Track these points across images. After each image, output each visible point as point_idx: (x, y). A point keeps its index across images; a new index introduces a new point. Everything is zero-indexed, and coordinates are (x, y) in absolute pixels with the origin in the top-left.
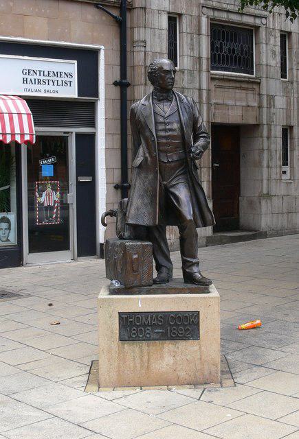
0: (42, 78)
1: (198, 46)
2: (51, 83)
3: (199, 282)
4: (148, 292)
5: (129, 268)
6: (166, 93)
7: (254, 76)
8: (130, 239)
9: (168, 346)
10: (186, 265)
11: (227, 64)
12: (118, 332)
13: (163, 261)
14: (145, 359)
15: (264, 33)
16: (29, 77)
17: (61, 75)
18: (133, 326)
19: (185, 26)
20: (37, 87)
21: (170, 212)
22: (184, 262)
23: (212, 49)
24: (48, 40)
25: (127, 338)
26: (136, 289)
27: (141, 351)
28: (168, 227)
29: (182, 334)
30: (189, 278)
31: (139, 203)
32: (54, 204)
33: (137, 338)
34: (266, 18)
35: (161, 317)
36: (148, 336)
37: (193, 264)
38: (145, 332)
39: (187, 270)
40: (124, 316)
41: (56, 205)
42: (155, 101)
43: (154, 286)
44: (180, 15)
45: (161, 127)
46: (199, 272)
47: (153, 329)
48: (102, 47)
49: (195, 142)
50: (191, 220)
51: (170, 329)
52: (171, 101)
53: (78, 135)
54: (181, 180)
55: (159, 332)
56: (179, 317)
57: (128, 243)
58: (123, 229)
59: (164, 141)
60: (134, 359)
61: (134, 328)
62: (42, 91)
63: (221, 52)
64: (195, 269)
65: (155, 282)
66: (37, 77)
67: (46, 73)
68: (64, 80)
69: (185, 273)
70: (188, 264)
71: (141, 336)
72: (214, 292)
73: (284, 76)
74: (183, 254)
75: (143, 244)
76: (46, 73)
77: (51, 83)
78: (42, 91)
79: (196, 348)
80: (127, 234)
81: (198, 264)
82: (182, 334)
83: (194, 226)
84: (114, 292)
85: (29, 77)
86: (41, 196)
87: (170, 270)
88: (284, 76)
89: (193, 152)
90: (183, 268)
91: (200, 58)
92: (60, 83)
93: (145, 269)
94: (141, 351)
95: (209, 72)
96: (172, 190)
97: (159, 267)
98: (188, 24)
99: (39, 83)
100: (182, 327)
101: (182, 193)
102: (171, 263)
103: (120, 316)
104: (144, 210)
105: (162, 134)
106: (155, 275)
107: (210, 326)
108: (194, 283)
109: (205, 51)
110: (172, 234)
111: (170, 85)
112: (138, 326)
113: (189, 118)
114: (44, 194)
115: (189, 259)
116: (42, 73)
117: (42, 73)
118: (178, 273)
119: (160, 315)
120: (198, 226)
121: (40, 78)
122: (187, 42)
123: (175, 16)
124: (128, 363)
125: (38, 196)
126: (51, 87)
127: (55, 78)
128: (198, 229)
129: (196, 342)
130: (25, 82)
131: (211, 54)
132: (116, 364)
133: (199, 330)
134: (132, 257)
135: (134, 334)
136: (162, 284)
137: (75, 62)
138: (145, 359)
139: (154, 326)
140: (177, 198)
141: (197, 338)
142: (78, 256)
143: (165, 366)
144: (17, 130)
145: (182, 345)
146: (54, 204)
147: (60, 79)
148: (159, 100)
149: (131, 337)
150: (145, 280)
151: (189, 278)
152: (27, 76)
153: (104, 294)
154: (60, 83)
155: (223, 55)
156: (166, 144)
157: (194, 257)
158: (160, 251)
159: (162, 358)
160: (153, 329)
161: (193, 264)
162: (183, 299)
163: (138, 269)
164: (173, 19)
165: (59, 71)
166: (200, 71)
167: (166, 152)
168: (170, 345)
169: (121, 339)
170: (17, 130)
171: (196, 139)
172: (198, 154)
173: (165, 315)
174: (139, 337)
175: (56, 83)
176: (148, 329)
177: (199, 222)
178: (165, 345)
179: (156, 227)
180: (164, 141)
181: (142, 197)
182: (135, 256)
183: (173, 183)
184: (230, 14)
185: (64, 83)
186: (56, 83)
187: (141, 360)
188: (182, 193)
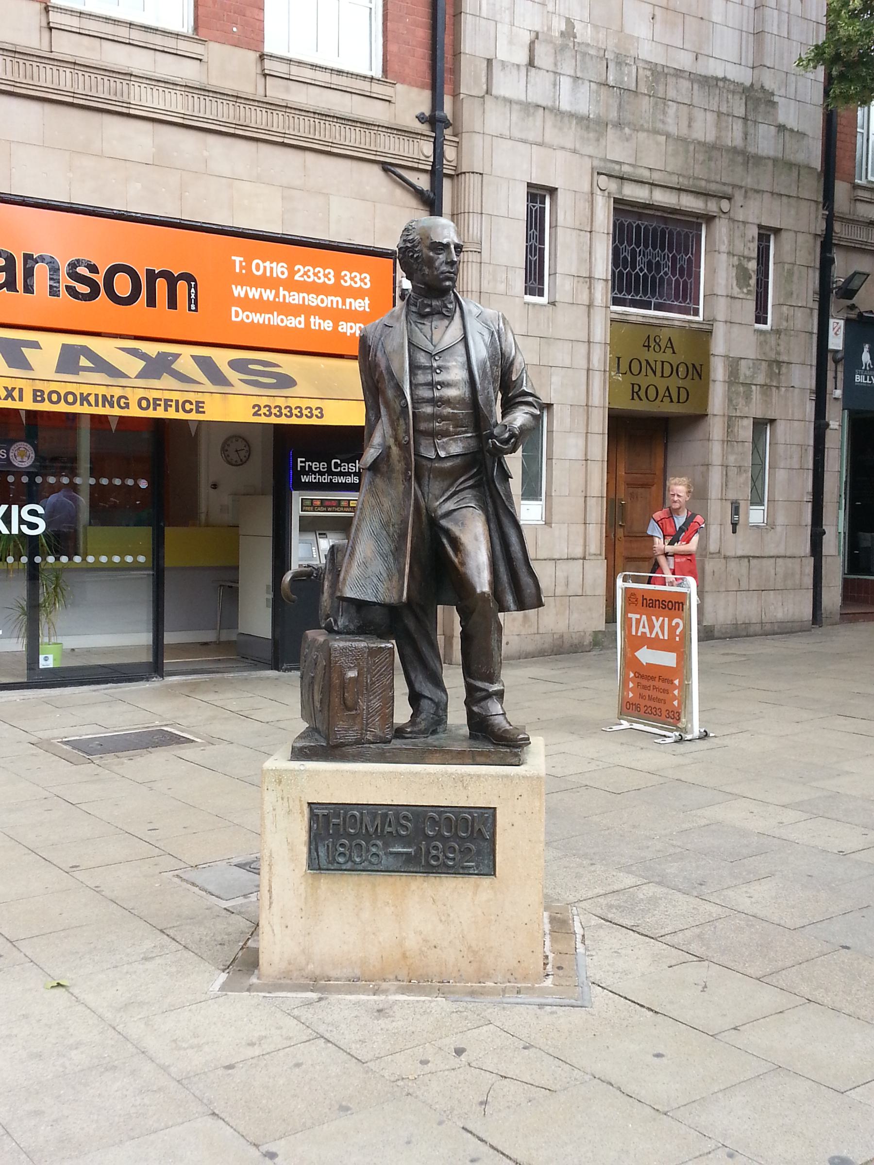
5: (336, 700)
6: (437, 297)
7: (700, 318)
8: (346, 632)
10: (474, 697)
11: (645, 293)
13: (426, 689)
18: (342, 836)
19: (564, 213)
22: (471, 690)
23: (615, 263)
26: (350, 750)
29: (454, 859)
31: (369, 553)
33: (349, 865)
34: (729, 199)
35: (405, 818)
37: (489, 696)
38: (368, 851)
39: (475, 709)
42: (414, 317)
43: (397, 743)
44: (552, 191)
45: (422, 378)
46: (506, 713)
49: (503, 417)
52: (451, 318)
54: (469, 499)
56: (448, 818)
57: (339, 644)
59: (428, 410)
61: (342, 839)
63: (634, 268)
64: (495, 707)
65: (399, 732)
69: (471, 715)
70: (479, 694)
73: (761, 318)
81: (500, 695)
82: (454, 859)
84: (300, 754)
87: (441, 708)
88: (761, 318)
89: (496, 438)
90: (466, 703)
93: (376, 704)
95: (607, 307)
96: (443, 522)
97: (415, 698)
100: (457, 843)
102: (444, 690)
103: (311, 810)
104: (378, 567)
105: (425, 393)
106: (402, 713)
108: (494, 741)
109: (603, 267)
110: (449, 621)
111: (449, 279)
113: (492, 357)
115: (479, 684)
118: (457, 716)
120: (503, 609)
123: (542, 192)
130: (193, 307)
131: (613, 273)
134: (342, 675)
136: (420, 739)
139: (389, 839)
140: (456, 543)
141: (491, 871)
148: (423, 316)
150: (376, 729)
153: (280, 761)
155: (637, 274)
156: (433, 417)
157: (492, 678)
158: (422, 664)
160: (386, 845)
161: (489, 696)
162: (461, 778)
164: (538, 195)
167: (433, 434)
169: (310, 867)
171: (508, 406)
172: (506, 442)
173: (349, 761)
174: (354, 862)
177: (509, 599)
180: (428, 410)
181: (377, 538)
182: (352, 674)
183: (450, 505)
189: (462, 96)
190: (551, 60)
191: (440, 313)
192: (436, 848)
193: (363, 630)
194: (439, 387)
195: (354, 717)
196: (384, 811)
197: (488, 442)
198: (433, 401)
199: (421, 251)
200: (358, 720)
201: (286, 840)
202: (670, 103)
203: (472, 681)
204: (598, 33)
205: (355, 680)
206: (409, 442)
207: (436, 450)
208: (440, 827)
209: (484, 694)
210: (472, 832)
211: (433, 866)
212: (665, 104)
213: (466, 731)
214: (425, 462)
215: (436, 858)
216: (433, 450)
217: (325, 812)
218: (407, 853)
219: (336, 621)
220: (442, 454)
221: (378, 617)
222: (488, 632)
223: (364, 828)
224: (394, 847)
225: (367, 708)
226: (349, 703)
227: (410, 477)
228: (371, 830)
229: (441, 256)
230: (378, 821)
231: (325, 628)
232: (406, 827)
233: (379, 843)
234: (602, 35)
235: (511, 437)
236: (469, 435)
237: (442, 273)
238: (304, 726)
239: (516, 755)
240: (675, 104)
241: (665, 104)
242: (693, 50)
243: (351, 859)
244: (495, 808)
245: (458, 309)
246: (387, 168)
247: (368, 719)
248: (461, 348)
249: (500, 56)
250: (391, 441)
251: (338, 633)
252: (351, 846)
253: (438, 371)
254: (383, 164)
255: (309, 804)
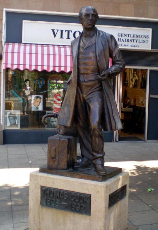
0: (129, 38)
2: (135, 41)
16: (122, 38)
17: (141, 37)
20: (126, 43)
24: (134, 17)
25: (45, 204)
26: (54, 171)
53: (151, 71)
55: (65, 205)
62: (130, 45)
66: (127, 38)
67: (132, 36)
68: (143, 39)
76: (132, 36)
77: (135, 41)
78: (130, 45)
85: (122, 38)
92: (141, 41)
99: (128, 41)
116: (130, 36)
117: (130, 36)
126: (135, 44)
127: (138, 39)
129: (88, 217)
130: (119, 41)
137: (151, 29)
142: (148, 139)
144: (57, 64)
147: (141, 39)
152: (121, 37)
154: (141, 41)
160: (60, 201)
170: (57, 64)
175: (138, 41)
185: (143, 41)
186: (138, 41)
188: (95, 107)
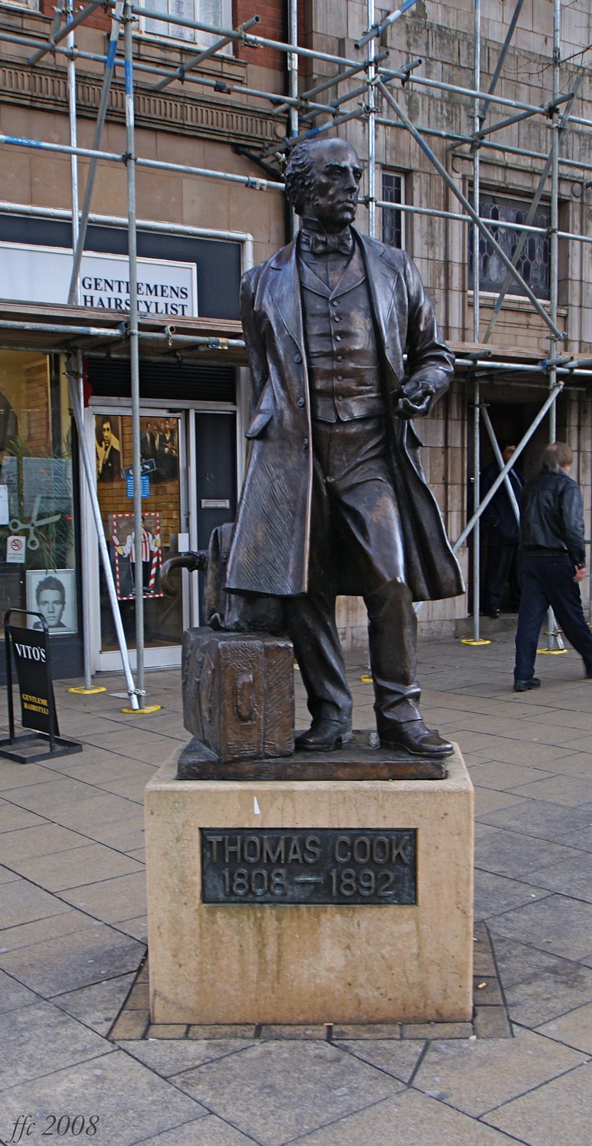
1: (442, 239)
3: (418, 750)
4: (281, 776)
6: (331, 232)
9: (333, 920)
10: (384, 700)
12: (197, 879)
14: (271, 952)
15: (577, 215)
17: (163, 291)
21: (340, 558)
22: (380, 692)
25: (221, 895)
26: (247, 766)
27: (260, 930)
28: (340, 599)
29: (369, 888)
30: (393, 736)
32: (151, 558)
35: (313, 843)
36: (278, 892)
37: (404, 700)
38: (270, 880)
39: (387, 715)
40: (214, 839)
41: (155, 560)
42: (307, 257)
43: (299, 759)
44: (517, 689)
46: (425, 717)
47: (291, 874)
48: (250, 237)
50: (402, 584)
51: (338, 877)
52: (349, 257)
58: (219, 605)
60: (242, 952)
68: (170, 301)
69: (382, 721)
71: (259, 891)
72: (460, 778)
74: (377, 672)
75: (267, 644)
79: (407, 927)
80: (233, 617)
82: (369, 888)
83: (408, 595)
84: (187, 773)
86: (123, 542)
90: (377, 708)
91: (447, 263)
94: (260, 930)
96: (348, 500)
98: (424, 191)
100: (377, 869)
101: (384, 514)
103: (205, 844)
106: (303, 720)
107: (447, 867)
108: (405, 750)
110: (352, 617)
112: (250, 866)
114: (130, 539)
118: (363, 719)
119: (310, 838)
120: (417, 598)
121: (118, 295)
122: (421, 230)
124: (224, 962)
125: (117, 543)
128: (418, 606)
130: (89, 299)
132: (193, 965)
133: (415, 878)
135: (241, 886)
136: (317, 751)
138: (271, 952)
139: (295, 868)
141: (413, 900)
143: (323, 973)
145: (368, 918)
146: (151, 558)
149: (232, 892)
151: (393, 736)
156: (330, 374)
159: (316, 949)
160: (291, 874)
163: (251, 712)
165: (159, 283)
166: (447, 289)
168: (338, 917)
169: (205, 899)
173: (326, 836)
174: (255, 894)
176: (278, 875)
177: (422, 586)
178: (324, 917)
179: (303, 597)
184: (509, 173)
187: (261, 953)
188: (384, 514)
189: (315, 76)
190: (404, 39)
191: (336, 252)
192: (349, 876)
193: (253, 626)
194: (339, 338)
195: (249, 728)
196: (288, 836)
197: (397, 403)
198: (331, 355)
199: (312, 176)
200: (254, 732)
201: (172, 866)
202: (521, 85)
203: (382, 683)
204: (448, 13)
205: (251, 686)
206: (304, 405)
207: (337, 413)
208: (352, 852)
209: (396, 698)
210: (391, 856)
211: (345, 897)
212: (516, 86)
213: (374, 739)
214: (323, 428)
215: (349, 887)
216: (333, 413)
217: (220, 838)
218: (315, 883)
219: (222, 617)
220: (346, 418)
221: (268, 611)
222: (400, 625)
223: (265, 855)
224: (299, 875)
225: (265, 717)
226: (245, 713)
227: (307, 447)
228: (274, 859)
229: (337, 182)
230: (281, 847)
231: (210, 625)
232: (314, 853)
233: (281, 871)
234: (452, 16)
235: (425, 394)
236: (373, 395)
237: (339, 202)
238: (189, 737)
239: (440, 768)
240: (526, 87)
241: (516, 86)
242: (542, 32)
243: (250, 891)
244: (415, 831)
245: (357, 247)
246: (237, 149)
247: (265, 730)
248: (363, 290)
249: (351, 36)
250: (282, 405)
251: (227, 630)
252: (250, 876)
253: (337, 319)
254: (232, 144)
255: (201, 829)
